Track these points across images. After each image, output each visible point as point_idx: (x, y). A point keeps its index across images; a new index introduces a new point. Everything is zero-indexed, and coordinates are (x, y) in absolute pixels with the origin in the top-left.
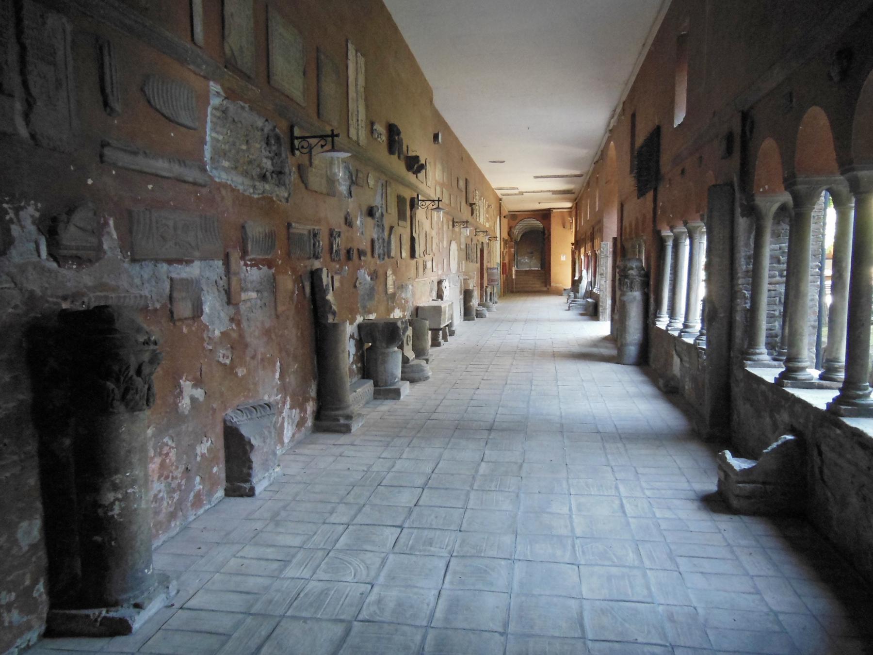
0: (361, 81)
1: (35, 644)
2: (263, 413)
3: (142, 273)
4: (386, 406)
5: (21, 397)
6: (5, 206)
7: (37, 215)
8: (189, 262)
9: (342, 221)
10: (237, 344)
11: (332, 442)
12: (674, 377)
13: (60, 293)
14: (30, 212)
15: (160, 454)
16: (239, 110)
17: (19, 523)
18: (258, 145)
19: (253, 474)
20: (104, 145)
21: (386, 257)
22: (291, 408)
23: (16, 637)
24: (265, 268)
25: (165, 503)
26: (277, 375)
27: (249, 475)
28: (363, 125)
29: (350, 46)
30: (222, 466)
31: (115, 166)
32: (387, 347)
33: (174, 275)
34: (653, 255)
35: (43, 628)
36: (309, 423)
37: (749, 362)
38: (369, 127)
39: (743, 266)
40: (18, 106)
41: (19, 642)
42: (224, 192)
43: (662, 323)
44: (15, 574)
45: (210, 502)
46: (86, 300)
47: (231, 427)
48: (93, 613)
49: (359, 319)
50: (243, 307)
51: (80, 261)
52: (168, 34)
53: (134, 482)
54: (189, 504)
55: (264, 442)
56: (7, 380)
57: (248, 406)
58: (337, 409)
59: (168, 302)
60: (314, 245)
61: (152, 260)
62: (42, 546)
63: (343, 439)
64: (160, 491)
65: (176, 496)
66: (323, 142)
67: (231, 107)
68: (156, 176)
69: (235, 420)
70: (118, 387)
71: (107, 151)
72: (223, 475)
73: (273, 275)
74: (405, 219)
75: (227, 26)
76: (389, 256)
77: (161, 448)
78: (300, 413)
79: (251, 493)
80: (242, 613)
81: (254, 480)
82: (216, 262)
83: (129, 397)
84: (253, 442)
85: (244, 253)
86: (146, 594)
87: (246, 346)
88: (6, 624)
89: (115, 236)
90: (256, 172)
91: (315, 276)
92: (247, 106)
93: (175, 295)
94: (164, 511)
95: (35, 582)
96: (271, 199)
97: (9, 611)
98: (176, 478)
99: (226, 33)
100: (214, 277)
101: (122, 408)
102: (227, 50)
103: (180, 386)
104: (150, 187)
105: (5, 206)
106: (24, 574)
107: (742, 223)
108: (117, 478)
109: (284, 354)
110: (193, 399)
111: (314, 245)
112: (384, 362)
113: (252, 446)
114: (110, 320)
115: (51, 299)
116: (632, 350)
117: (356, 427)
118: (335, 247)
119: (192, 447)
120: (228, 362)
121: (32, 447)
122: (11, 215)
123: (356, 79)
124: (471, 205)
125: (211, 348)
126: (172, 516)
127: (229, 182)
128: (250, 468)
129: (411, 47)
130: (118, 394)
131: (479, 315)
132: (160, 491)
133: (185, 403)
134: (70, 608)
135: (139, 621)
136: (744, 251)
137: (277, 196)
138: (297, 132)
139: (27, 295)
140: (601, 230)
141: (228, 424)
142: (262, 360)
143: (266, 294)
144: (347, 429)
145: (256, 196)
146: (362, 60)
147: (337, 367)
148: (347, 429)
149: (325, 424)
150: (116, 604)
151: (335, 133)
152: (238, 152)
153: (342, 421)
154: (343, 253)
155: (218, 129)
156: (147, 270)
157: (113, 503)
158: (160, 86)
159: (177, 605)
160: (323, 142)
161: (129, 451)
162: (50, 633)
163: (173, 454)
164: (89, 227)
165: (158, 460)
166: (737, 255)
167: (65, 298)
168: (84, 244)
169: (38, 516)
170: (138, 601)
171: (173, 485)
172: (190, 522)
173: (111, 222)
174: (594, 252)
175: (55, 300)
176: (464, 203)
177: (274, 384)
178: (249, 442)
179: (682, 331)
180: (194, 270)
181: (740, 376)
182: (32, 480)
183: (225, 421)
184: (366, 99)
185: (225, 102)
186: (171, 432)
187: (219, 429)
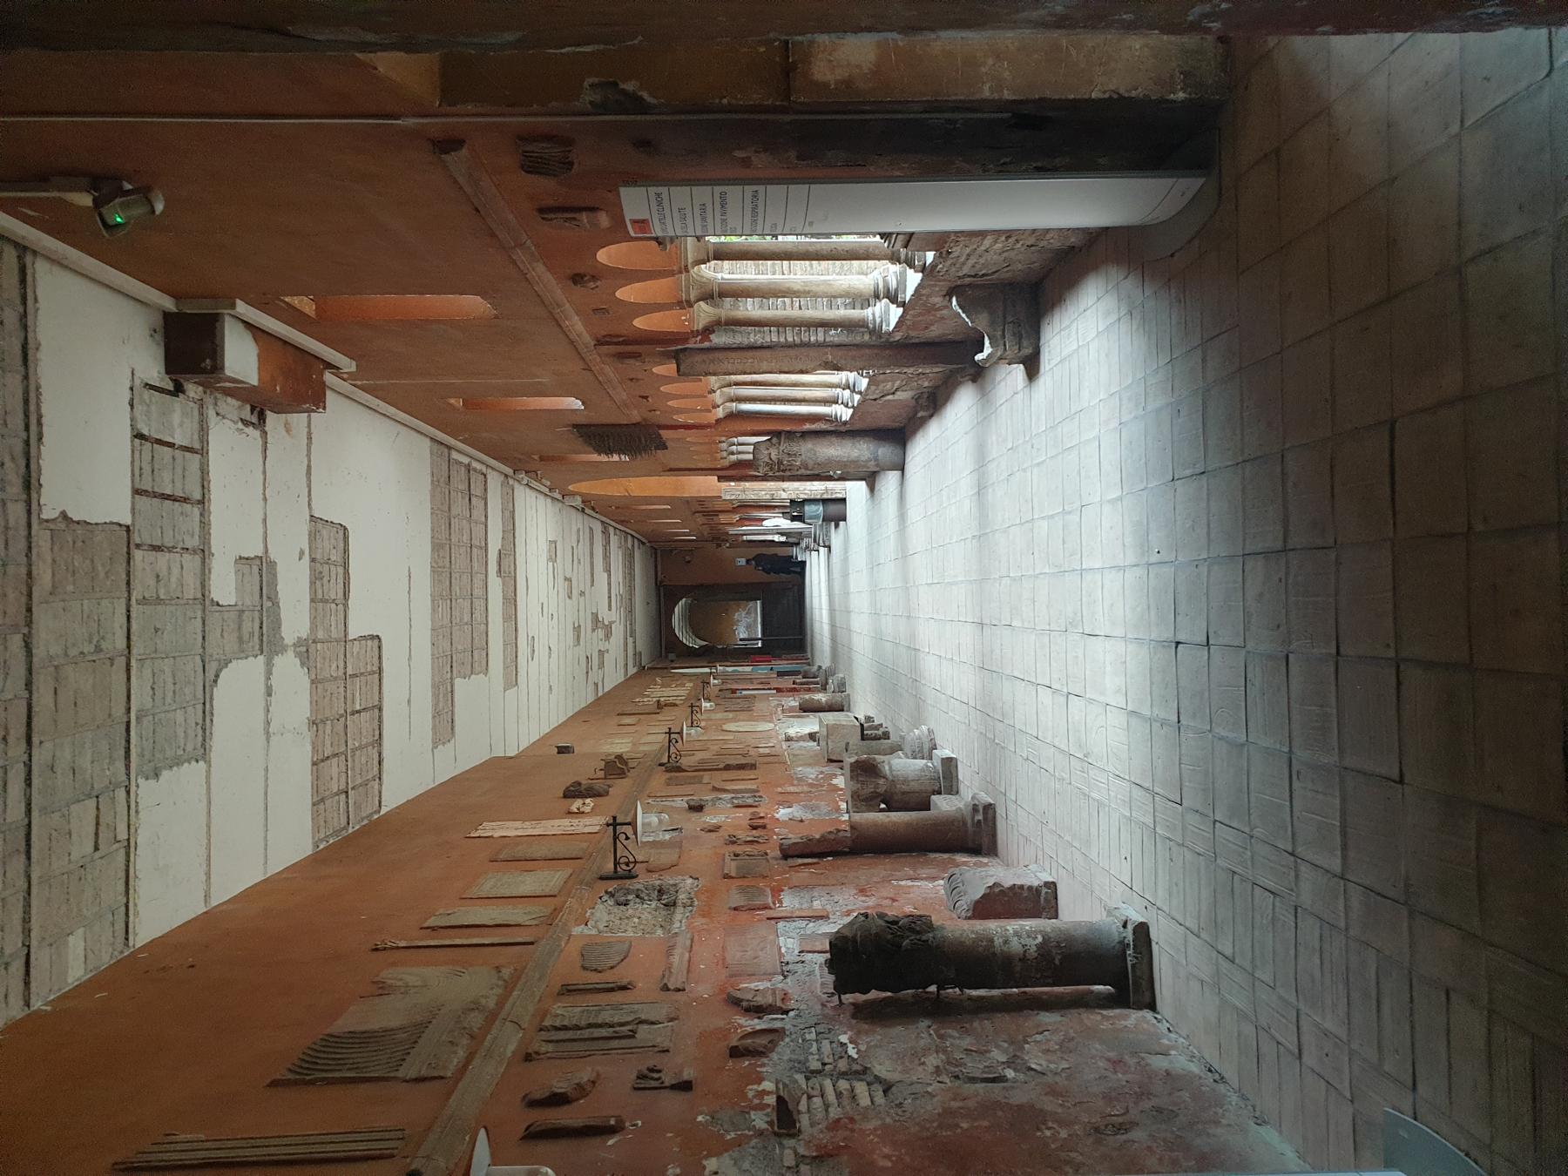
0: (518, 824)
9: (713, 835)
12: (917, 399)
27: (1030, 888)
34: (749, 427)
43: (846, 414)
58: (965, 823)
63: (1000, 812)
66: (622, 837)
79: (1052, 886)
81: (1036, 883)
107: (718, 339)
112: (906, 781)
116: (885, 452)
128: (1022, 887)
131: (842, 687)
136: (754, 337)
138: (665, 760)
140: (701, 501)
148: (989, 809)
149: (985, 840)
153: (980, 817)
160: (622, 837)
162: (1152, 1007)
170: (1120, 925)
174: (734, 510)
176: (660, 717)
179: (853, 391)
181: (898, 336)
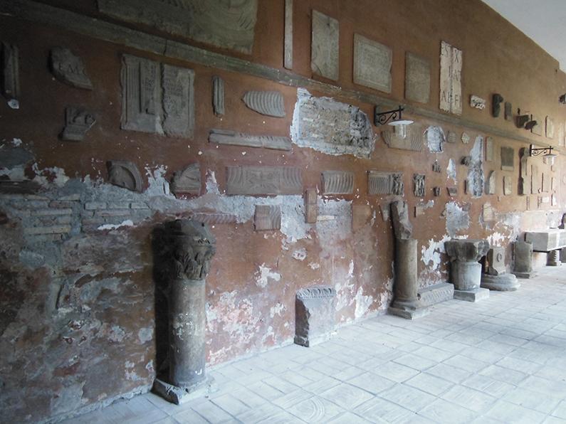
1: (145, 394)
3: (234, 202)
4: (462, 304)
5: (146, 264)
6: (146, 168)
7: (165, 172)
8: (273, 196)
10: (312, 247)
11: (391, 323)
13: (175, 212)
14: (161, 170)
15: (240, 308)
16: (325, 102)
17: (140, 328)
19: (309, 332)
20: (211, 133)
22: (364, 294)
23: (133, 387)
25: (242, 338)
26: (351, 271)
28: (458, 98)
29: (443, 45)
30: (293, 323)
31: (217, 143)
32: (467, 261)
33: (259, 204)
35: (151, 387)
36: (384, 307)
38: (467, 99)
40: (158, 119)
41: (134, 390)
42: (305, 153)
44: (136, 353)
45: (280, 344)
46: (191, 216)
47: (299, 300)
48: (167, 386)
49: (446, 238)
50: (319, 225)
51: (189, 196)
52: (262, 67)
53: (190, 320)
54: (262, 342)
55: (321, 313)
56: (139, 254)
58: (405, 301)
59: (253, 220)
60: (394, 185)
61: (242, 195)
62: (153, 343)
64: (238, 330)
65: (252, 335)
67: (318, 101)
68: (247, 148)
69: (303, 296)
70: (183, 265)
71: (212, 136)
72: (294, 329)
73: (351, 205)
74: (510, 163)
76: (487, 193)
77: (241, 305)
78: (374, 299)
80: (232, 415)
82: (296, 196)
83: (187, 271)
85: (322, 191)
86: (194, 385)
87: (321, 250)
88: (128, 378)
89: (215, 181)
90: (343, 139)
91: (392, 208)
93: (257, 216)
94: (240, 342)
95: (147, 361)
97: (130, 372)
98: (252, 324)
99: (313, 58)
100: (294, 205)
101: (184, 277)
102: (313, 66)
103: (259, 269)
104: (244, 153)
105: (146, 168)
106: (141, 355)
108: (181, 315)
109: (358, 258)
110: (269, 279)
111: (394, 185)
112: (464, 272)
113: (309, 315)
114: (179, 228)
115: (168, 215)
117: (416, 316)
119: (267, 309)
120: (302, 259)
121: (152, 290)
122: (149, 172)
123: (451, 67)
125: (287, 249)
126: (247, 346)
128: (308, 328)
129: (526, 33)
130: (183, 268)
132: (238, 330)
133: (262, 281)
134: (162, 380)
135: (184, 399)
139: (155, 212)
141: (298, 298)
142: (336, 260)
143: (343, 217)
144: (408, 317)
147: (406, 271)
148: (408, 317)
149: (395, 310)
150: (177, 385)
151: (402, 108)
153: (407, 310)
155: (309, 115)
156: (239, 200)
157: (178, 329)
158: (262, 97)
159: (209, 398)
161: (189, 302)
163: (250, 310)
164: (195, 177)
165: (238, 311)
167: (178, 215)
168: (190, 186)
169: (151, 327)
170: (188, 388)
171: (248, 328)
172: (261, 354)
173: (213, 174)
175: (172, 215)
177: (347, 277)
178: (308, 311)
180: (279, 200)
182: (150, 308)
185: (312, 99)
186: (249, 296)
187: (292, 300)
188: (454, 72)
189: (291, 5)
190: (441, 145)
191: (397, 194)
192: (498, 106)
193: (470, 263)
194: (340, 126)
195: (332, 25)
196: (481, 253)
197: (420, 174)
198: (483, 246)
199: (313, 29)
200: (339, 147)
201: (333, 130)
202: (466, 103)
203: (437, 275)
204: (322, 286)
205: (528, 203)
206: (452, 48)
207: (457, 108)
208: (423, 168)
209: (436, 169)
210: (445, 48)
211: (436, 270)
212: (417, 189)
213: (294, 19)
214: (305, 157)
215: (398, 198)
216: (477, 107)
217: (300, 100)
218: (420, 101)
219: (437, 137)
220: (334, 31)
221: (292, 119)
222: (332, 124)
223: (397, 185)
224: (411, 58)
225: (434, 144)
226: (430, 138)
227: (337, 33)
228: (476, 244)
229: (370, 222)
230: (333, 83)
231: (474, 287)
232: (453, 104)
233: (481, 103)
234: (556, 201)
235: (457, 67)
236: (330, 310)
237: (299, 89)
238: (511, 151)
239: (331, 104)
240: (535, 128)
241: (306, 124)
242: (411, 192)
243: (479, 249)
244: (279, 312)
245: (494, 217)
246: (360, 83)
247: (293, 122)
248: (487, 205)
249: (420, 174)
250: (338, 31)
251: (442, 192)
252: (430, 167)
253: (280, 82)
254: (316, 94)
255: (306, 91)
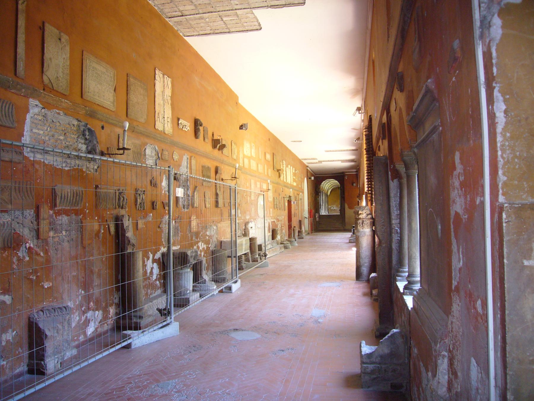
2: (60, 313)
16: (56, 115)
18: (73, 136)
19: (46, 355)
21: (190, 207)
24: (74, 216)
27: (43, 356)
28: (169, 120)
29: (157, 72)
37: (399, 278)
39: (395, 212)
42: (37, 166)
55: (58, 333)
57: (50, 308)
60: (119, 199)
75: (45, 65)
76: (193, 207)
84: (48, 333)
85: (53, 205)
91: (118, 219)
92: (61, 112)
96: (81, 170)
99: (45, 70)
107: (393, 185)
111: (119, 199)
118: (139, 201)
123: (163, 92)
124: (278, 170)
127: (42, 160)
137: (87, 168)
145: (67, 169)
146: (168, 81)
152: (56, 141)
154: (148, 205)
155: (39, 127)
166: (391, 204)
183: (29, 318)
184: (172, 105)
185: (43, 110)
187: (24, 322)
188: (165, 96)
189: (24, 15)
190: (157, 162)
191: (122, 208)
192: (199, 129)
193: (183, 271)
194: (69, 139)
195: (63, 40)
196: (193, 262)
197: (140, 189)
198: (194, 254)
199: (46, 42)
200: (69, 161)
201: (62, 143)
202: (176, 125)
203: (156, 285)
204: (55, 305)
205: (222, 214)
206: (164, 75)
207: (168, 128)
208: (143, 184)
209: (154, 184)
210: (159, 74)
211: (156, 280)
212: (139, 203)
213: (27, 28)
214: (37, 170)
215: (123, 212)
216: (184, 129)
217: (31, 111)
218: (140, 121)
219: (153, 154)
220: (65, 46)
221: (24, 130)
222: (62, 138)
223: (122, 199)
224: (131, 80)
225: (151, 161)
226: (148, 155)
227: (68, 48)
228: (189, 253)
229: (98, 237)
230: (64, 96)
231: (188, 292)
232: (166, 125)
233: (187, 125)
234: (241, 213)
235: (168, 92)
236: (66, 328)
237: (31, 100)
238: (209, 169)
239: (62, 117)
240: (225, 150)
241: (36, 135)
242: (133, 206)
243: (191, 257)
244: (11, 338)
245: (198, 228)
246: (88, 99)
247: (25, 133)
248: (193, 217)
249: (140, 189)
250: (69, 46)
251: (159, 206)
252: (149, 182)
253: (13, 91)
254: (46, 106)
255: (37, 102)
